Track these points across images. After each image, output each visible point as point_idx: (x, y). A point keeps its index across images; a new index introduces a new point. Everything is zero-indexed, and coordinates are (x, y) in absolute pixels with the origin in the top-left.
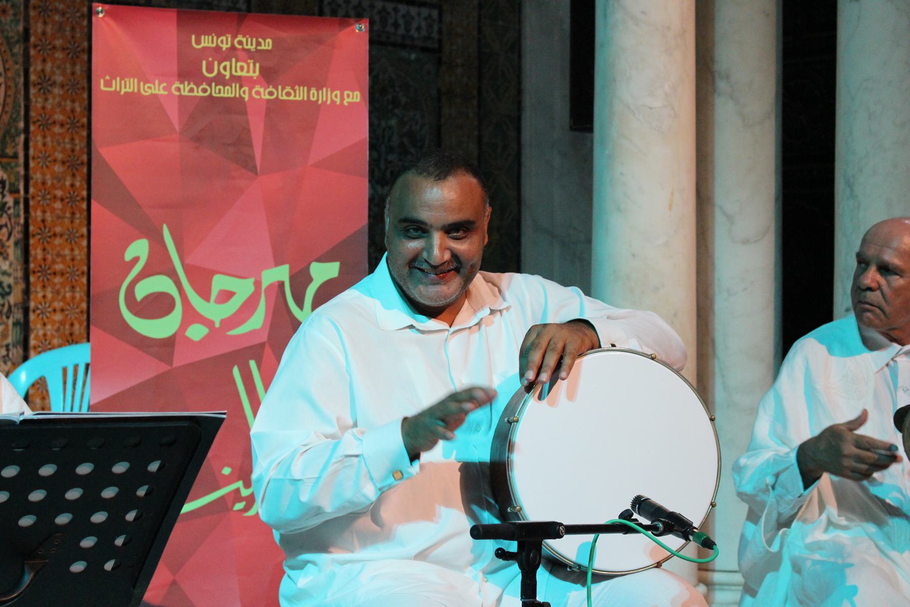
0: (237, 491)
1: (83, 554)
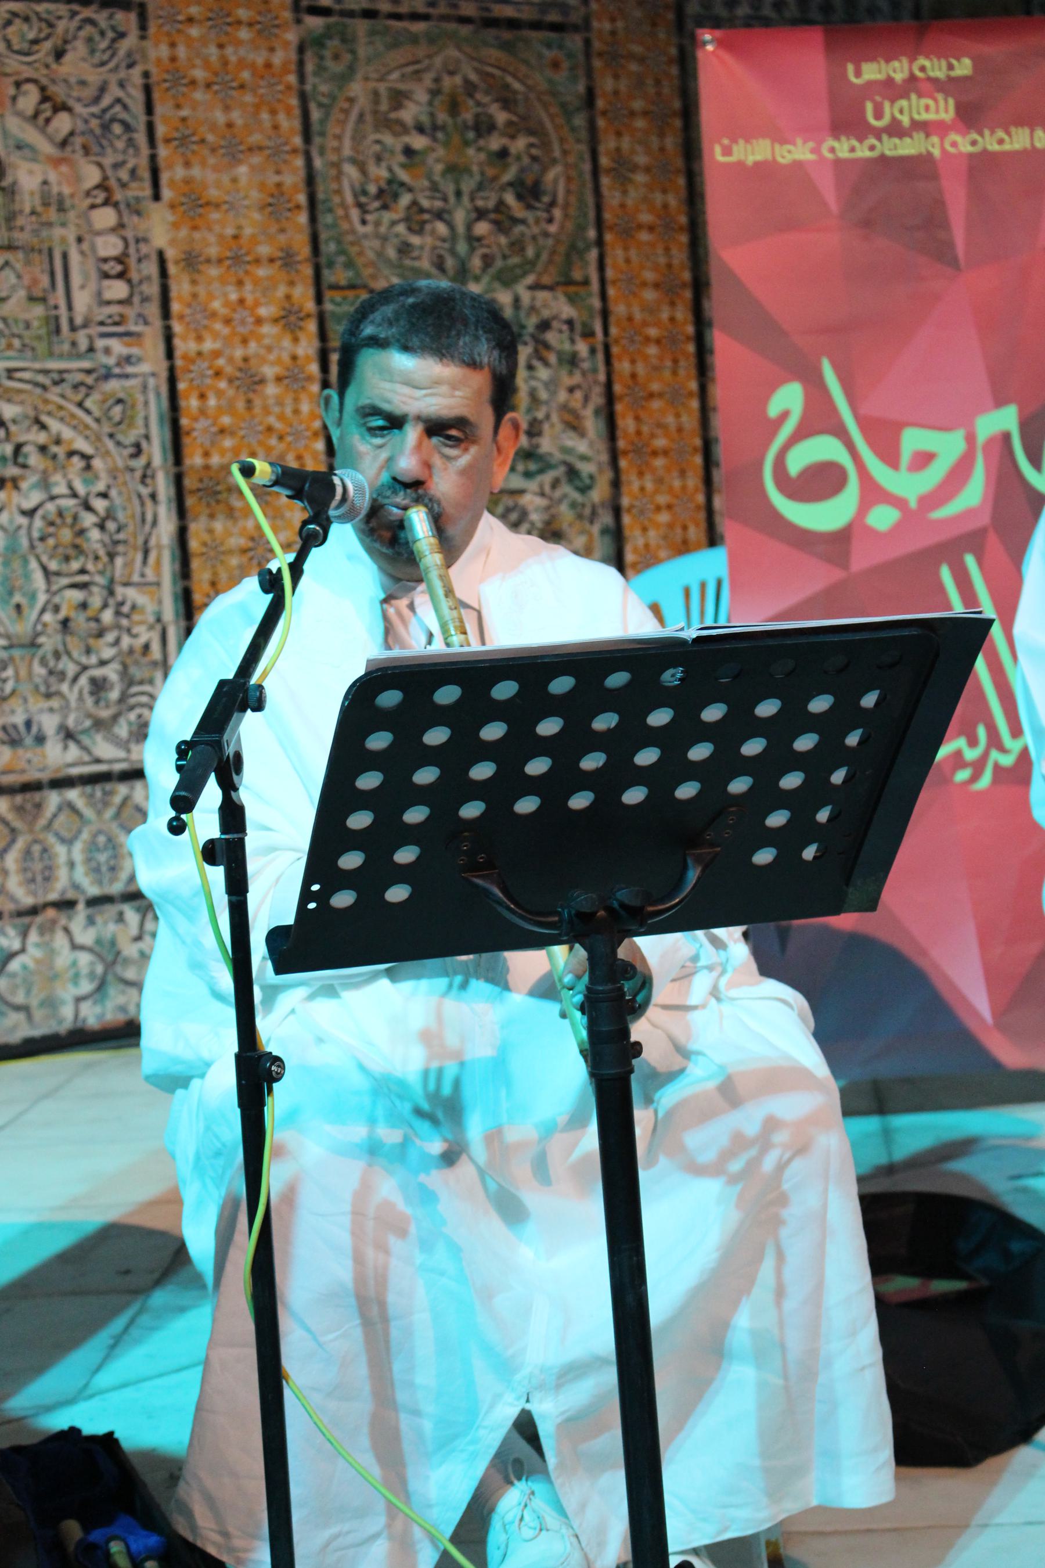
0: (958, 754)
1: (770, 838)
